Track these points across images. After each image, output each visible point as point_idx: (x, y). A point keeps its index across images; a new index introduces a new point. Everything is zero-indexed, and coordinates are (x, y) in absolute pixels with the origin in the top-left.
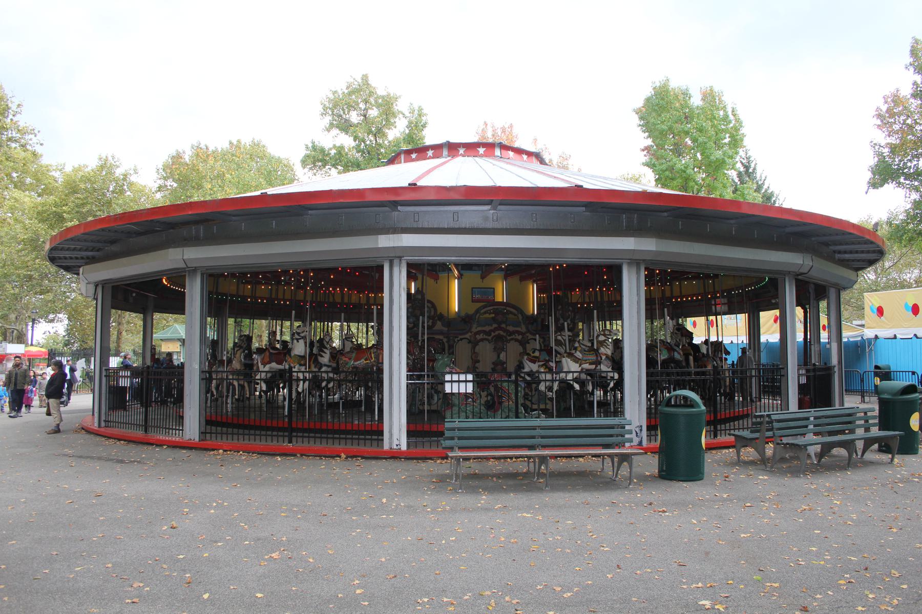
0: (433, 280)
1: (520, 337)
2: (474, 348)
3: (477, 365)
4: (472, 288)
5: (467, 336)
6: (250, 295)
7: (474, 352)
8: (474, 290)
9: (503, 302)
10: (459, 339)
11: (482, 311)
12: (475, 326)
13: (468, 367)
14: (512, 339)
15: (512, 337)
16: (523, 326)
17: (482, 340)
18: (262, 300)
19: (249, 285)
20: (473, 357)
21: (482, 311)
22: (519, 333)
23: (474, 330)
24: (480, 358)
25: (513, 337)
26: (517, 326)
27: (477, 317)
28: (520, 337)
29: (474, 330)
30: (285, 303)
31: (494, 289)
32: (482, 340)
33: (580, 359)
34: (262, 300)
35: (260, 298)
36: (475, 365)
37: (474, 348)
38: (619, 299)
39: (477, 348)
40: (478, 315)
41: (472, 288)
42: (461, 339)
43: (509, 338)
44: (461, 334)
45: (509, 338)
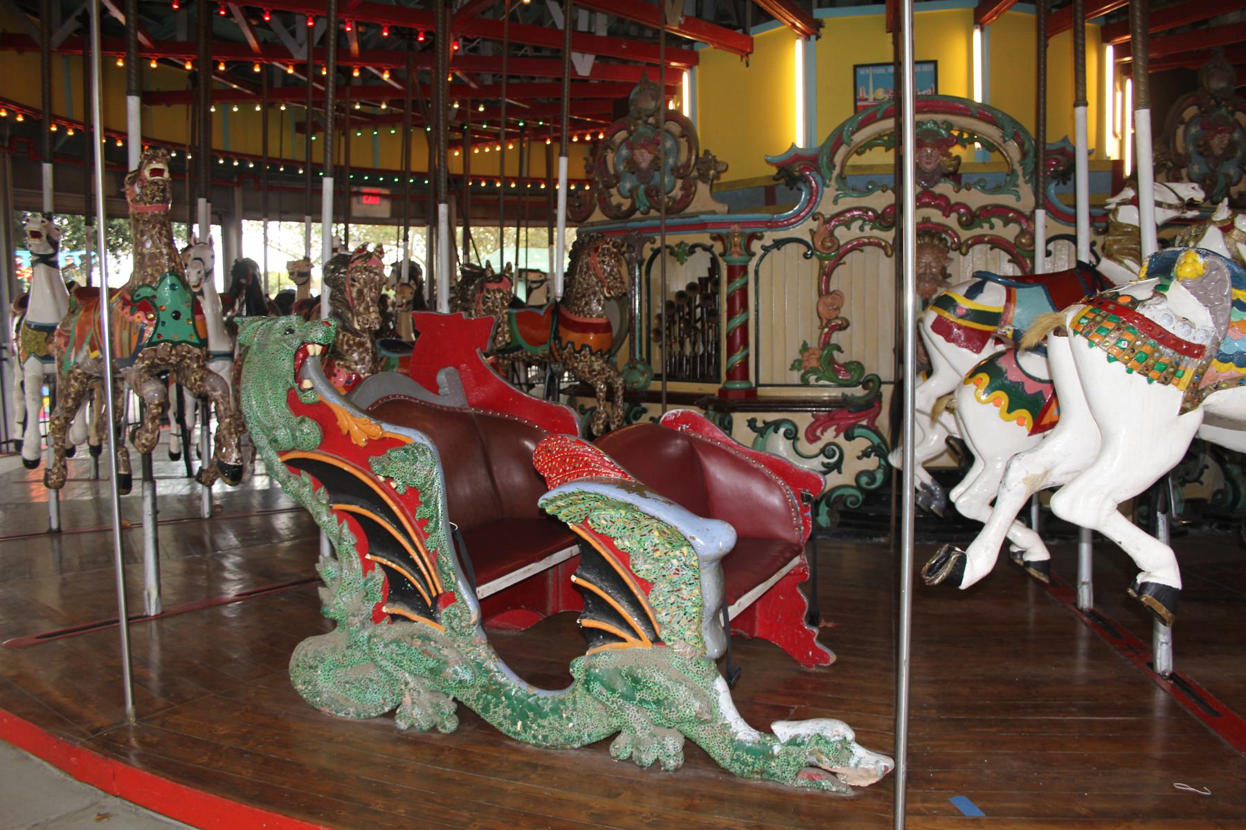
0: (738, 57)
1: (1010, 232)
2: (826, 275)
3: (837, 338)
4: (856, 67)
5: (801, 230)
6: (516, 174)
7: (828, 292)
8: (861, 72)
9: (968, 102)
10: (768, 242)
11: (860, 137)
12: (829, 192)
13: (805, 344)
14: (979, 240)
15: (977, 231)
16: (1026, 190)
17: (858, 246)
18: (229, 161)
19: (457, 149)
20: (821, 309)
21: (860, 137)
22: (1001, 211)
23: (827, 207)
24: (848, 311)
25: (985, 230)
26: (998, 189)
27: (838, 159)
28: (1010, 232)
29: (827, 207)
30: (62, 130)
31: (935, 63)
32: (858, 246)
33: (1192, 350)
34: (229, 161)
35: (487, 178)
36: (828, 335)
37: (826, 275)
38: (908, 818)
39: (839, 272)
40: (843, 150)
41: (856, 67)
42: (778, 244)
43: (965, 235)
44: (773, 225)
45: (965, 235)
